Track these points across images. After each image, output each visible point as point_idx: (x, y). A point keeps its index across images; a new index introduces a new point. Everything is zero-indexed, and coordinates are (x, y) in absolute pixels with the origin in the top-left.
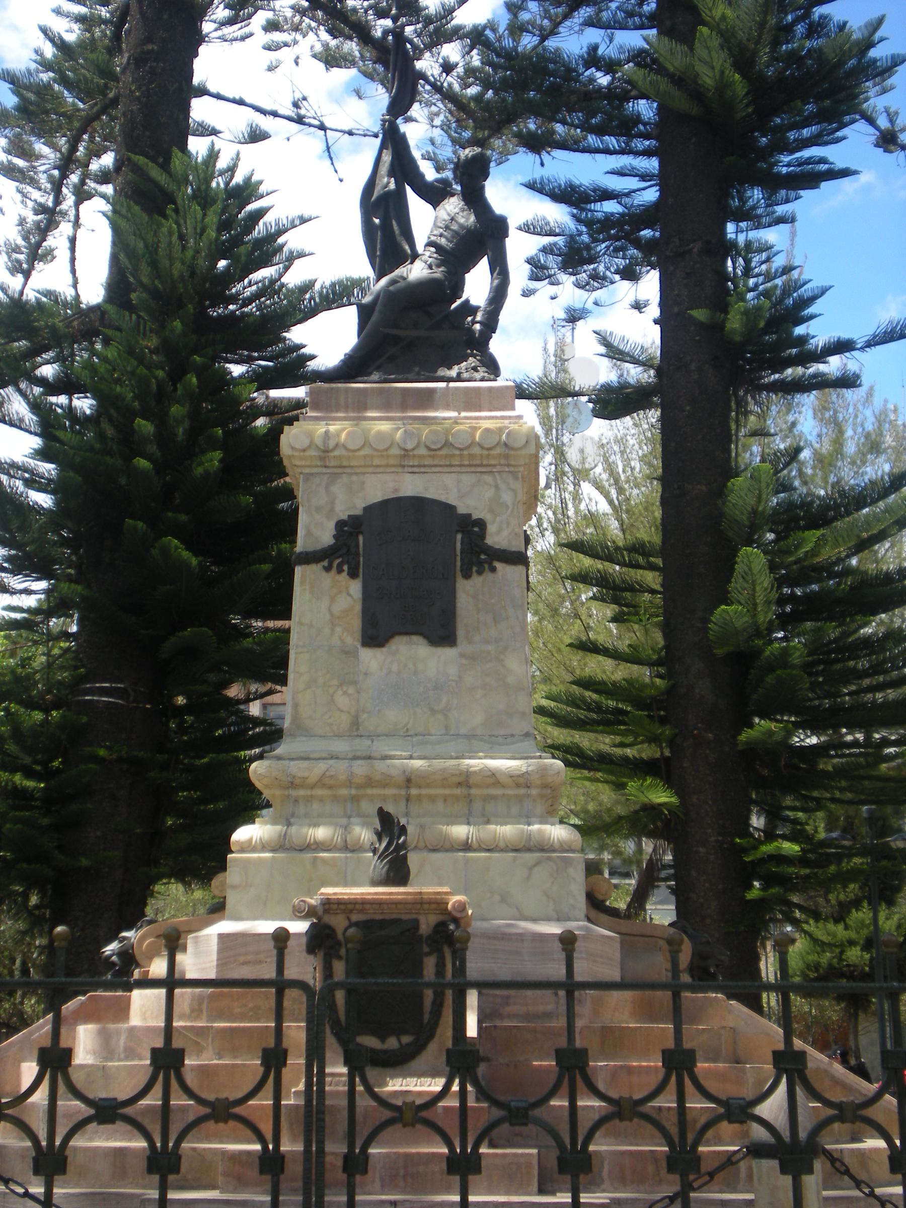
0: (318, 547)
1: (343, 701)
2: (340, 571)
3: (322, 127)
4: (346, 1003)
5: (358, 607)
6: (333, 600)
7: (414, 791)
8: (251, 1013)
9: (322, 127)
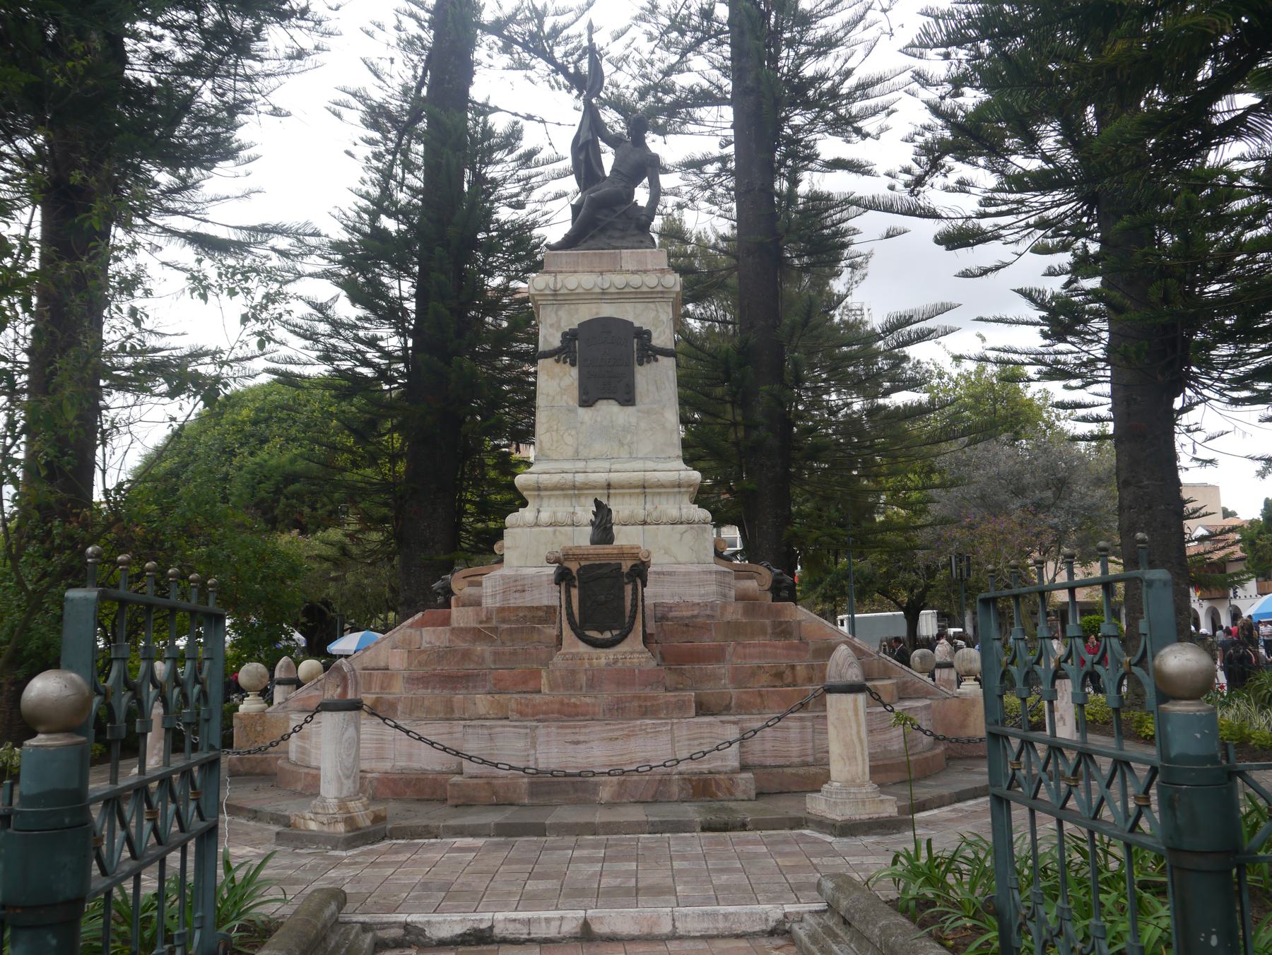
0: (551, 348)
1: (569, 440)
2: (565, 362)
3: (543, 121)
5: (576, 384)
6: (561, 379)
7: (612, 491)
9: (543, 121)
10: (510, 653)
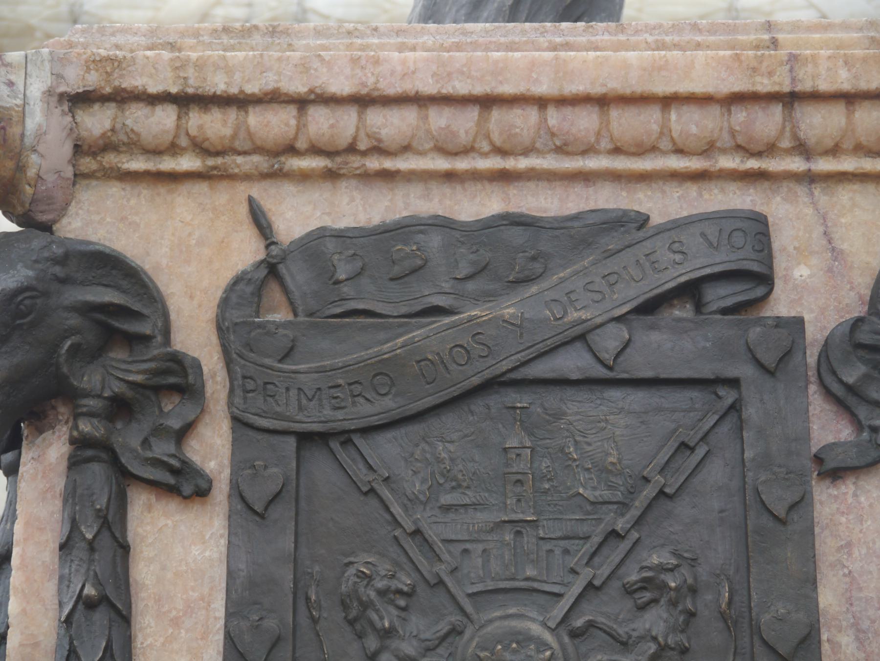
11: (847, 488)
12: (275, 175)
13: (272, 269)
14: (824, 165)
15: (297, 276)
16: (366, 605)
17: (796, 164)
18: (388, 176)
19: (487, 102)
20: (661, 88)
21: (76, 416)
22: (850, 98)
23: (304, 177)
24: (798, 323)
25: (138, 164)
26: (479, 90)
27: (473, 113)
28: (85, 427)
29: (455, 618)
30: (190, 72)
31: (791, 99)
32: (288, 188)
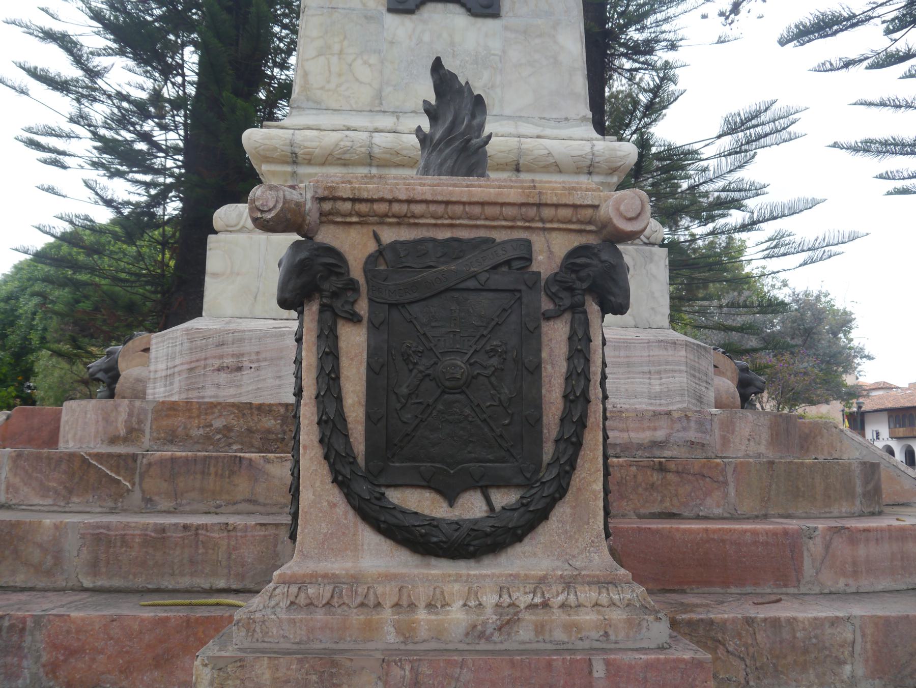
1: (363, 72)
4: (368, 416)
8: (218, 436)
10: (147, 542)
11: (551, 323)
12: (382, 223)
13: (380, 252)
14: (548, 225)
15: (389, 255)
16: (409, 355)
17: (540, 225)
18: (416, 224)
19: (447, 203)
20: (500, 200)
21: (321, 297)
22: (556, 206)
23: (390, 224)
24: (539, 273)
25: (339, 219)
26: (445, 199)
27: (443, 206)
28: (325, 300)
29: (436, 359)
30: (356, 191)
31: (539, 205)
32: (386, 227)
